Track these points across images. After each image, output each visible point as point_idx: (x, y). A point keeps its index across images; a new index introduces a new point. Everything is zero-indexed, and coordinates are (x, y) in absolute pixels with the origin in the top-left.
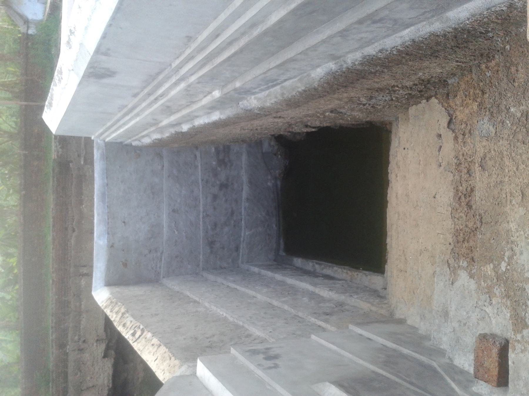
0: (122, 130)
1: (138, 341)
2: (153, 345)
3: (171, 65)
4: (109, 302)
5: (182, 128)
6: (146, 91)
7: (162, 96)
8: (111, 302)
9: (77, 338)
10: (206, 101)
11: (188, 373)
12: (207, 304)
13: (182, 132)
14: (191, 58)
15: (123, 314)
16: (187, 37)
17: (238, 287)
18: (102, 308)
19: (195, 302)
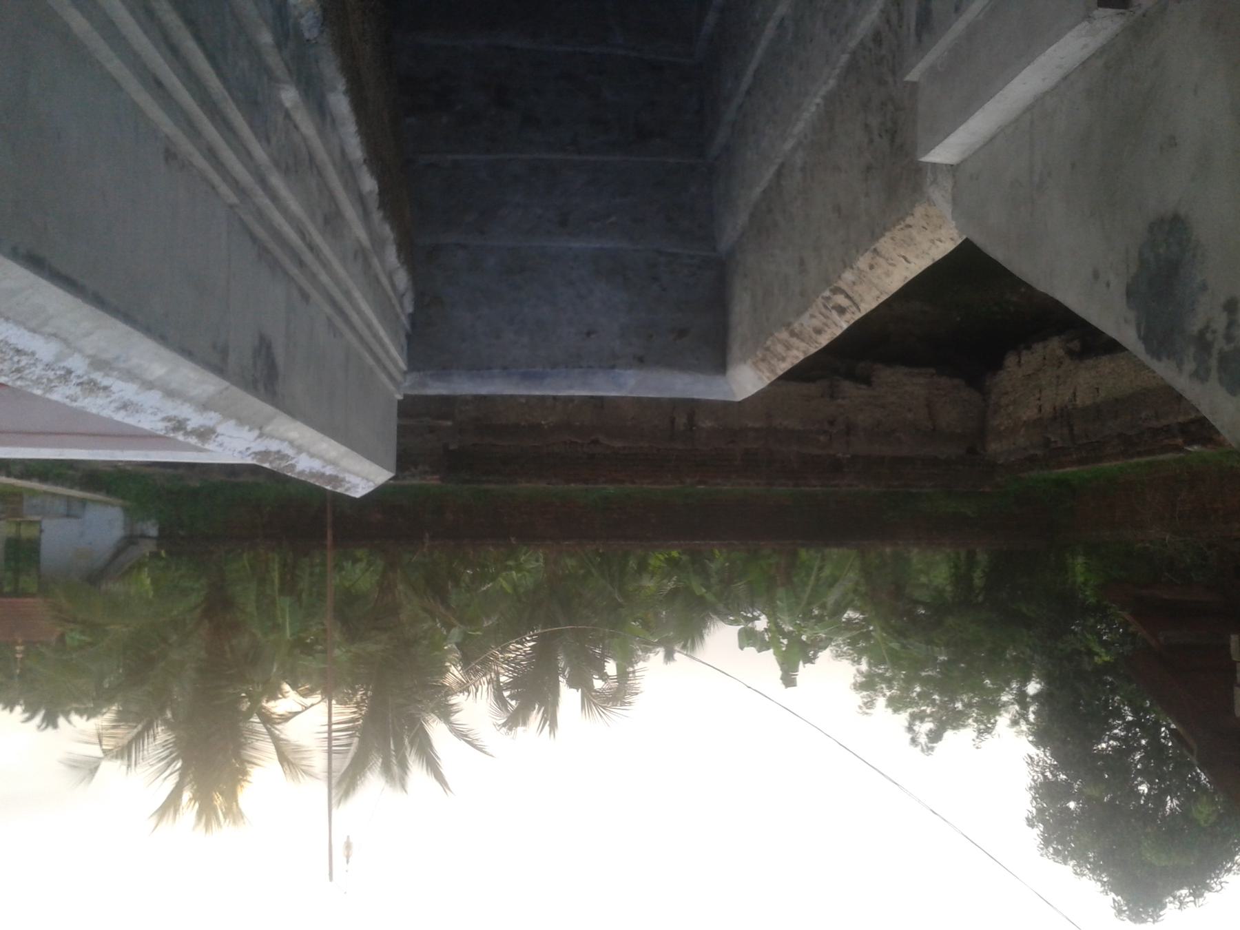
0: (382, 333)
1: (856, 298)
2: (871, 267)
3: (231, 207)
4: (763, 366)
5: (371, 192)
6: (294, 271)
7: (303, 234)
8: (763, 360)
9: (822, 438)
10: (306, 125)
11: (948, 184)
12: (789, 145)
13: (381, 193)
14: (211, 154)
15: (793, 334)
16: (166, 159)
17: (753, 66)
18: (774, 378)
19: (779, 174)
